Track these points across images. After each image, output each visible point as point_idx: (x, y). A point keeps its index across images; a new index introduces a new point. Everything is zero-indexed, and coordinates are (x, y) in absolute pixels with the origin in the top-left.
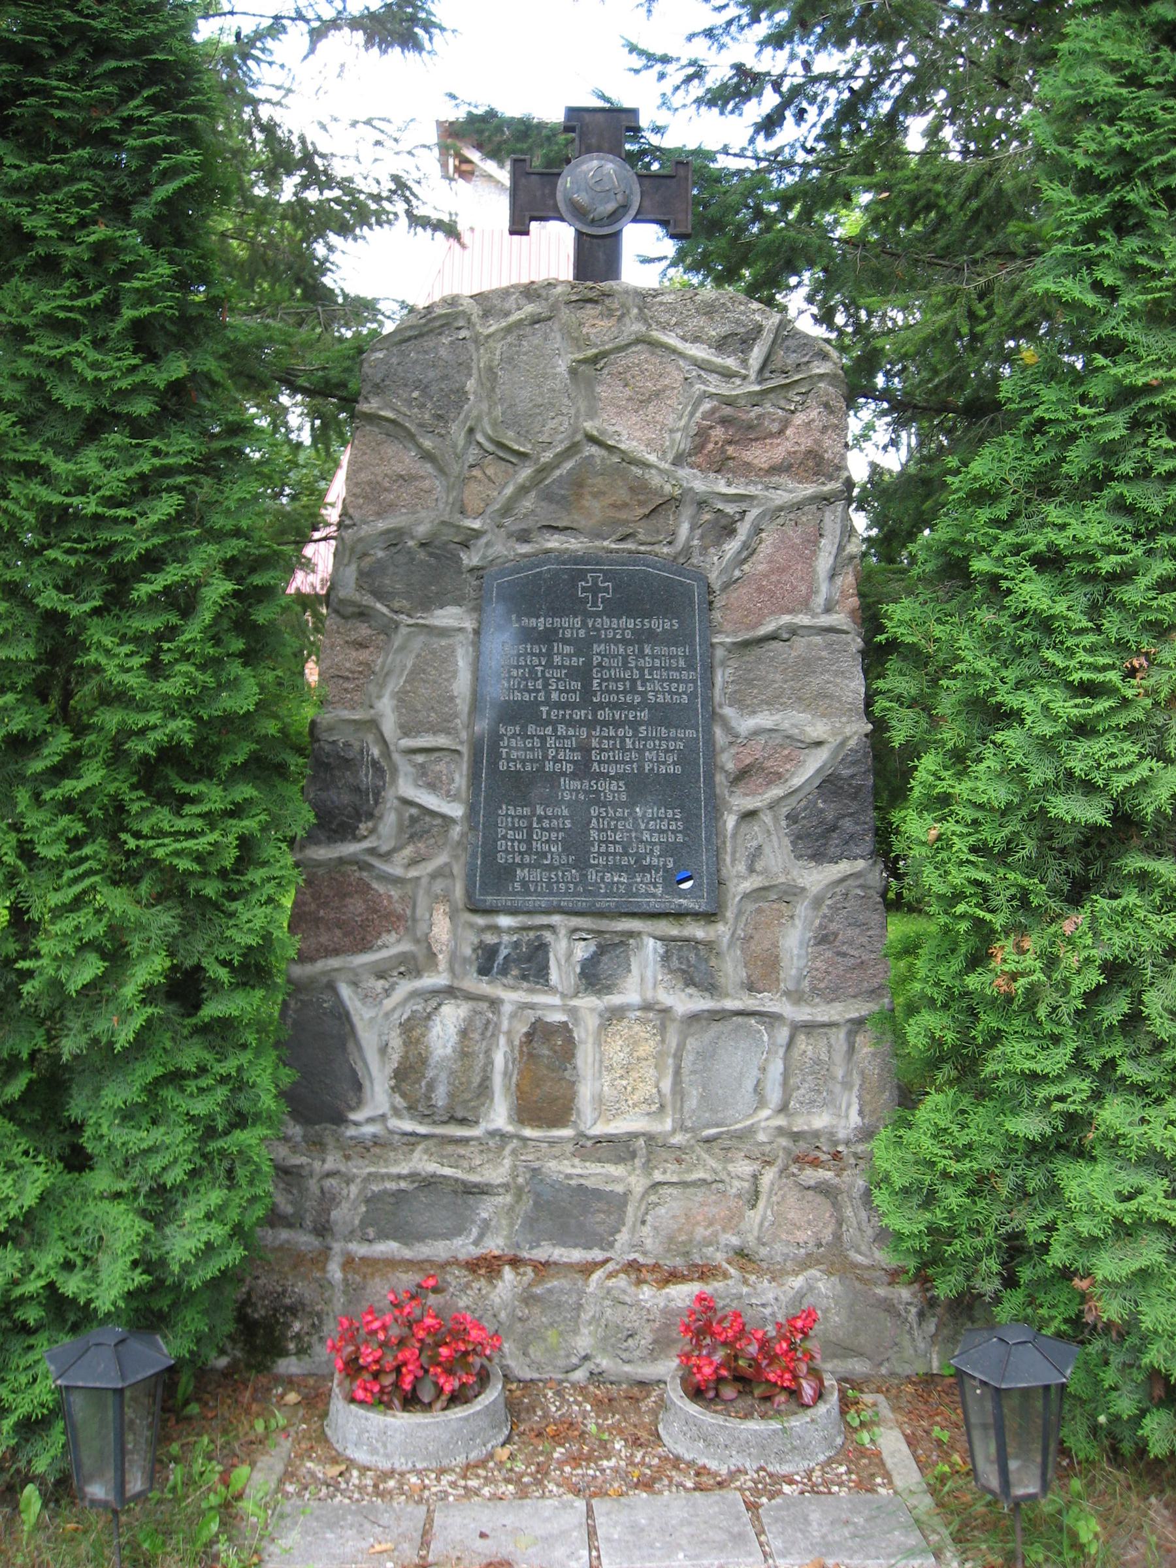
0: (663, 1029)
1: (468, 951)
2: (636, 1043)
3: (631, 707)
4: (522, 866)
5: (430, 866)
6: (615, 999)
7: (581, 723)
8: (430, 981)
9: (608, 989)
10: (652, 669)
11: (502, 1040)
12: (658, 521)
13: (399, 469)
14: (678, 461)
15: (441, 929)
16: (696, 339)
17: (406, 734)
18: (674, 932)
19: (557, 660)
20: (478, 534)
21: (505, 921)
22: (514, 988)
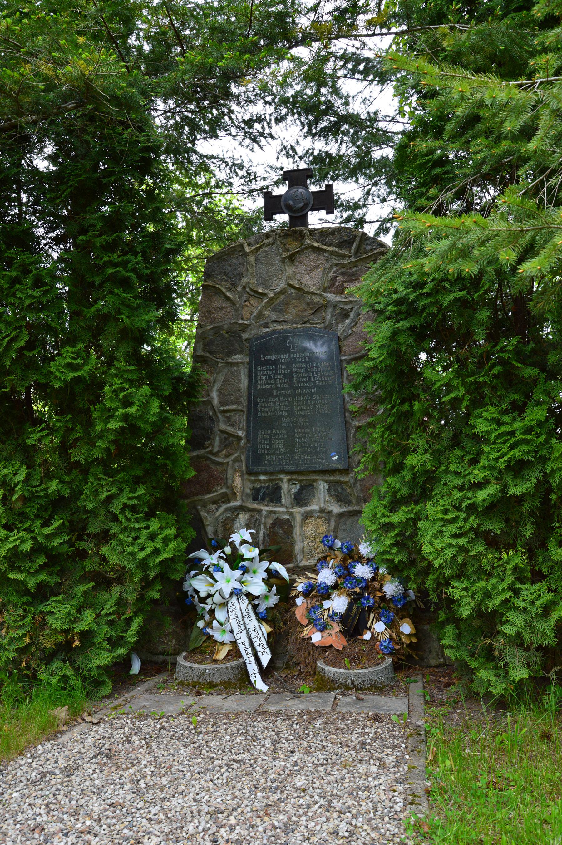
0: (329, 520)
1: (249, 491)
2: (318, 527)
3: (309, 387)
4: (268, 454)
5: (232, 458)
6: (308, 508)
7: (289, 396)
8: (233, 504)
9: (306, 505)
10: (317, 372)
11: (262, 527)
12: (318, 315)
13: (218, 305)
14: (325, 290)
15: (238, 482)
16: (330, 245)
17: (222, 406)
18: (332, 478)
19: (279, 371)
20: (247, 326)
21: (262, 478)
22: (266, 506)
